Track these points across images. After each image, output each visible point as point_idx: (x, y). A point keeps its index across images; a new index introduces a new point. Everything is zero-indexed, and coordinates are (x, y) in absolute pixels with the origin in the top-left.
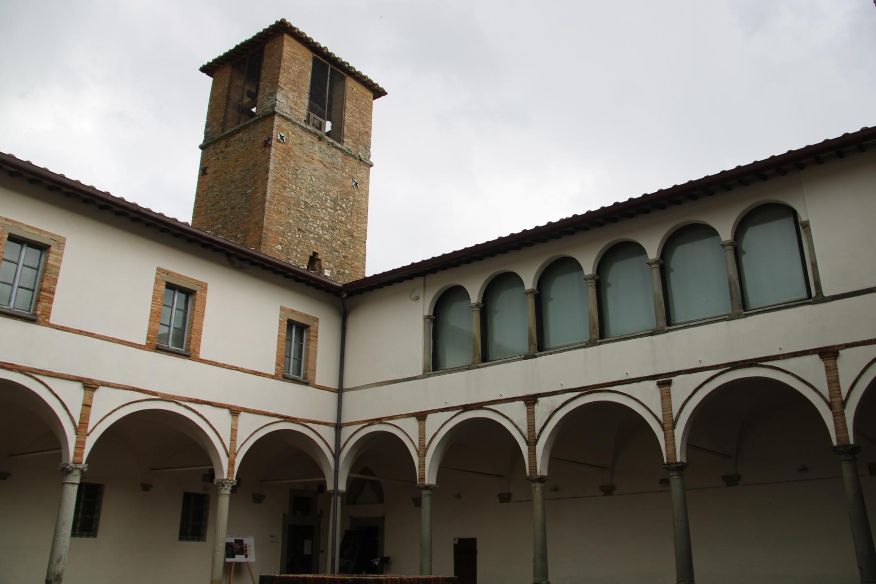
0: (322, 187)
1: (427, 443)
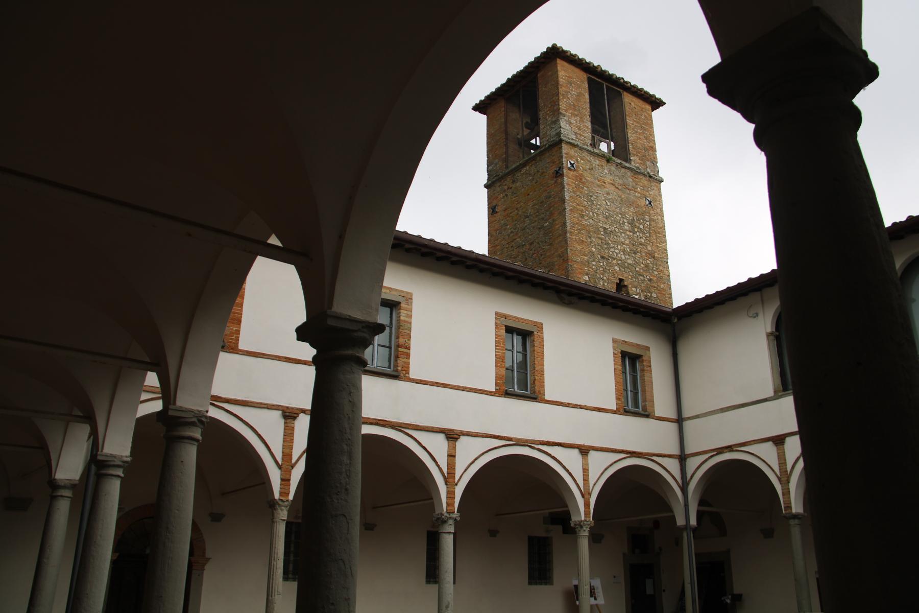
0: (618, 210)
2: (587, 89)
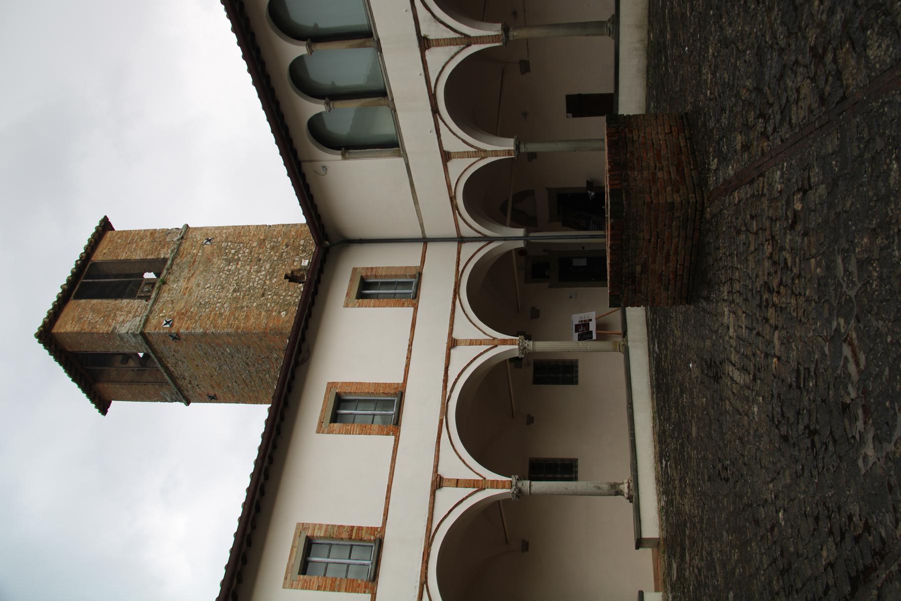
0: (215, 276)
1: (473, 150)
2: (86, 300)
